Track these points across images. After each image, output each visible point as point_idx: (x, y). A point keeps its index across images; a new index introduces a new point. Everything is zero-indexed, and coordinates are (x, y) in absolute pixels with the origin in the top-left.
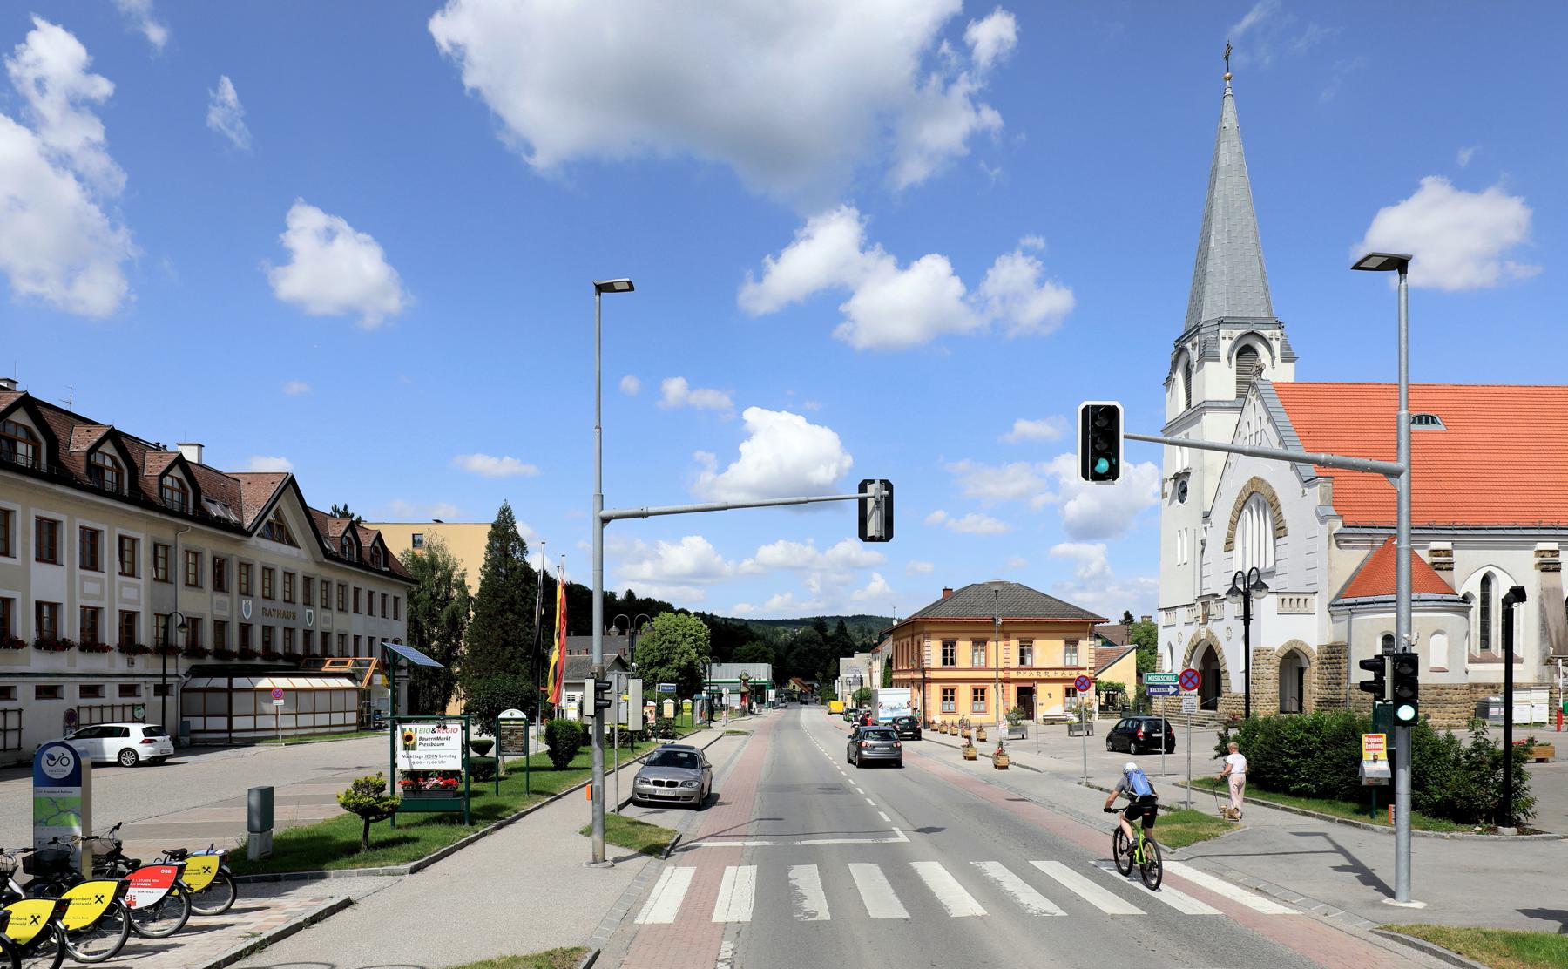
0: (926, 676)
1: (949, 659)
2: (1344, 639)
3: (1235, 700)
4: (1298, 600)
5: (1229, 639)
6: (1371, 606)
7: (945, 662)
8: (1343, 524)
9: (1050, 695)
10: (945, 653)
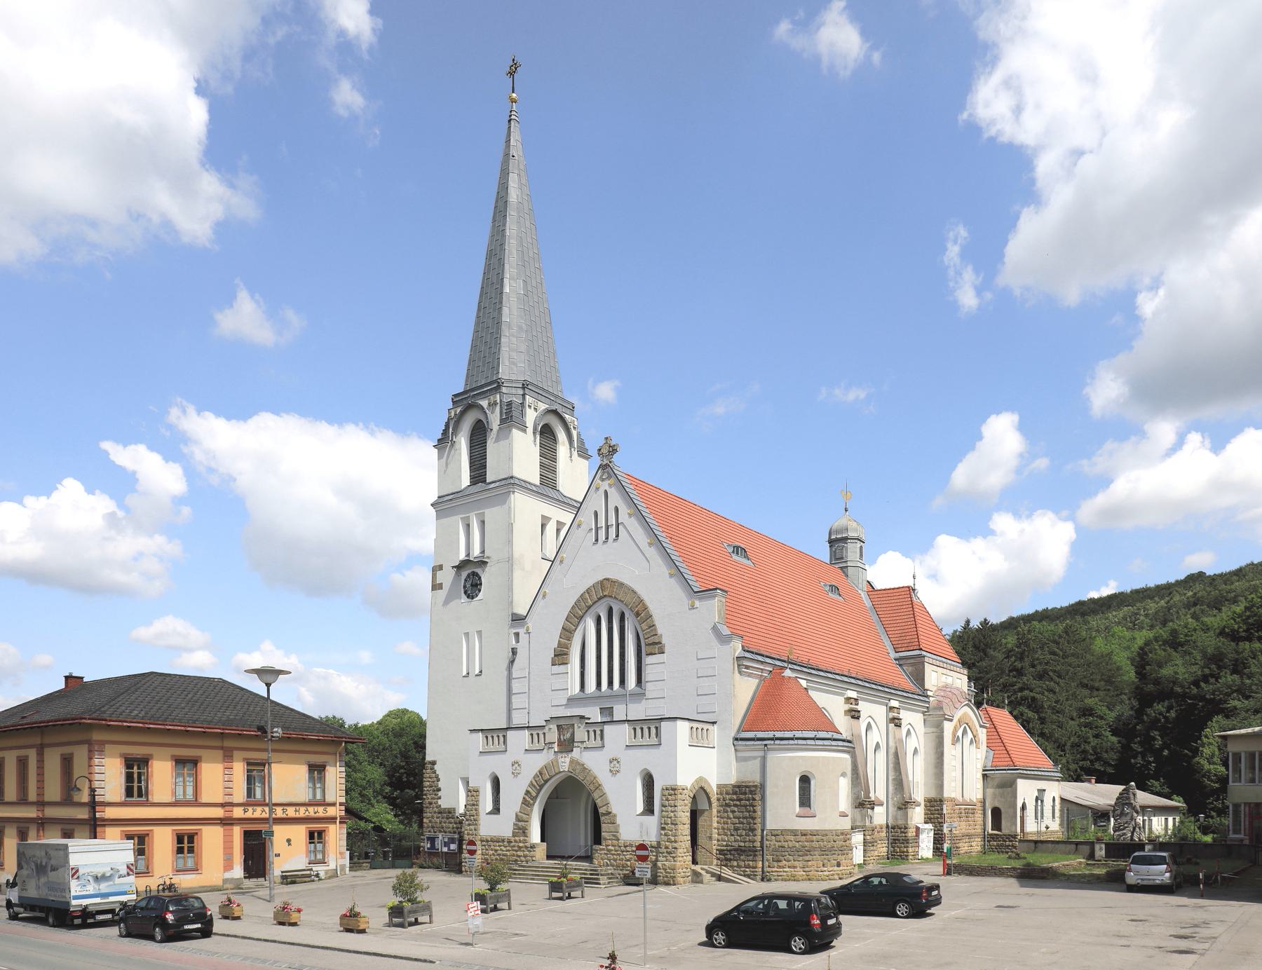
0: (98, 815)
1: (135, 789)
2: (755, 778)
4: (702, 729)
5: (614, 772)
6: (791, 742)
7: (129, 792)
8: (743, 646)
9: (289, 841)
10: (129, 778)
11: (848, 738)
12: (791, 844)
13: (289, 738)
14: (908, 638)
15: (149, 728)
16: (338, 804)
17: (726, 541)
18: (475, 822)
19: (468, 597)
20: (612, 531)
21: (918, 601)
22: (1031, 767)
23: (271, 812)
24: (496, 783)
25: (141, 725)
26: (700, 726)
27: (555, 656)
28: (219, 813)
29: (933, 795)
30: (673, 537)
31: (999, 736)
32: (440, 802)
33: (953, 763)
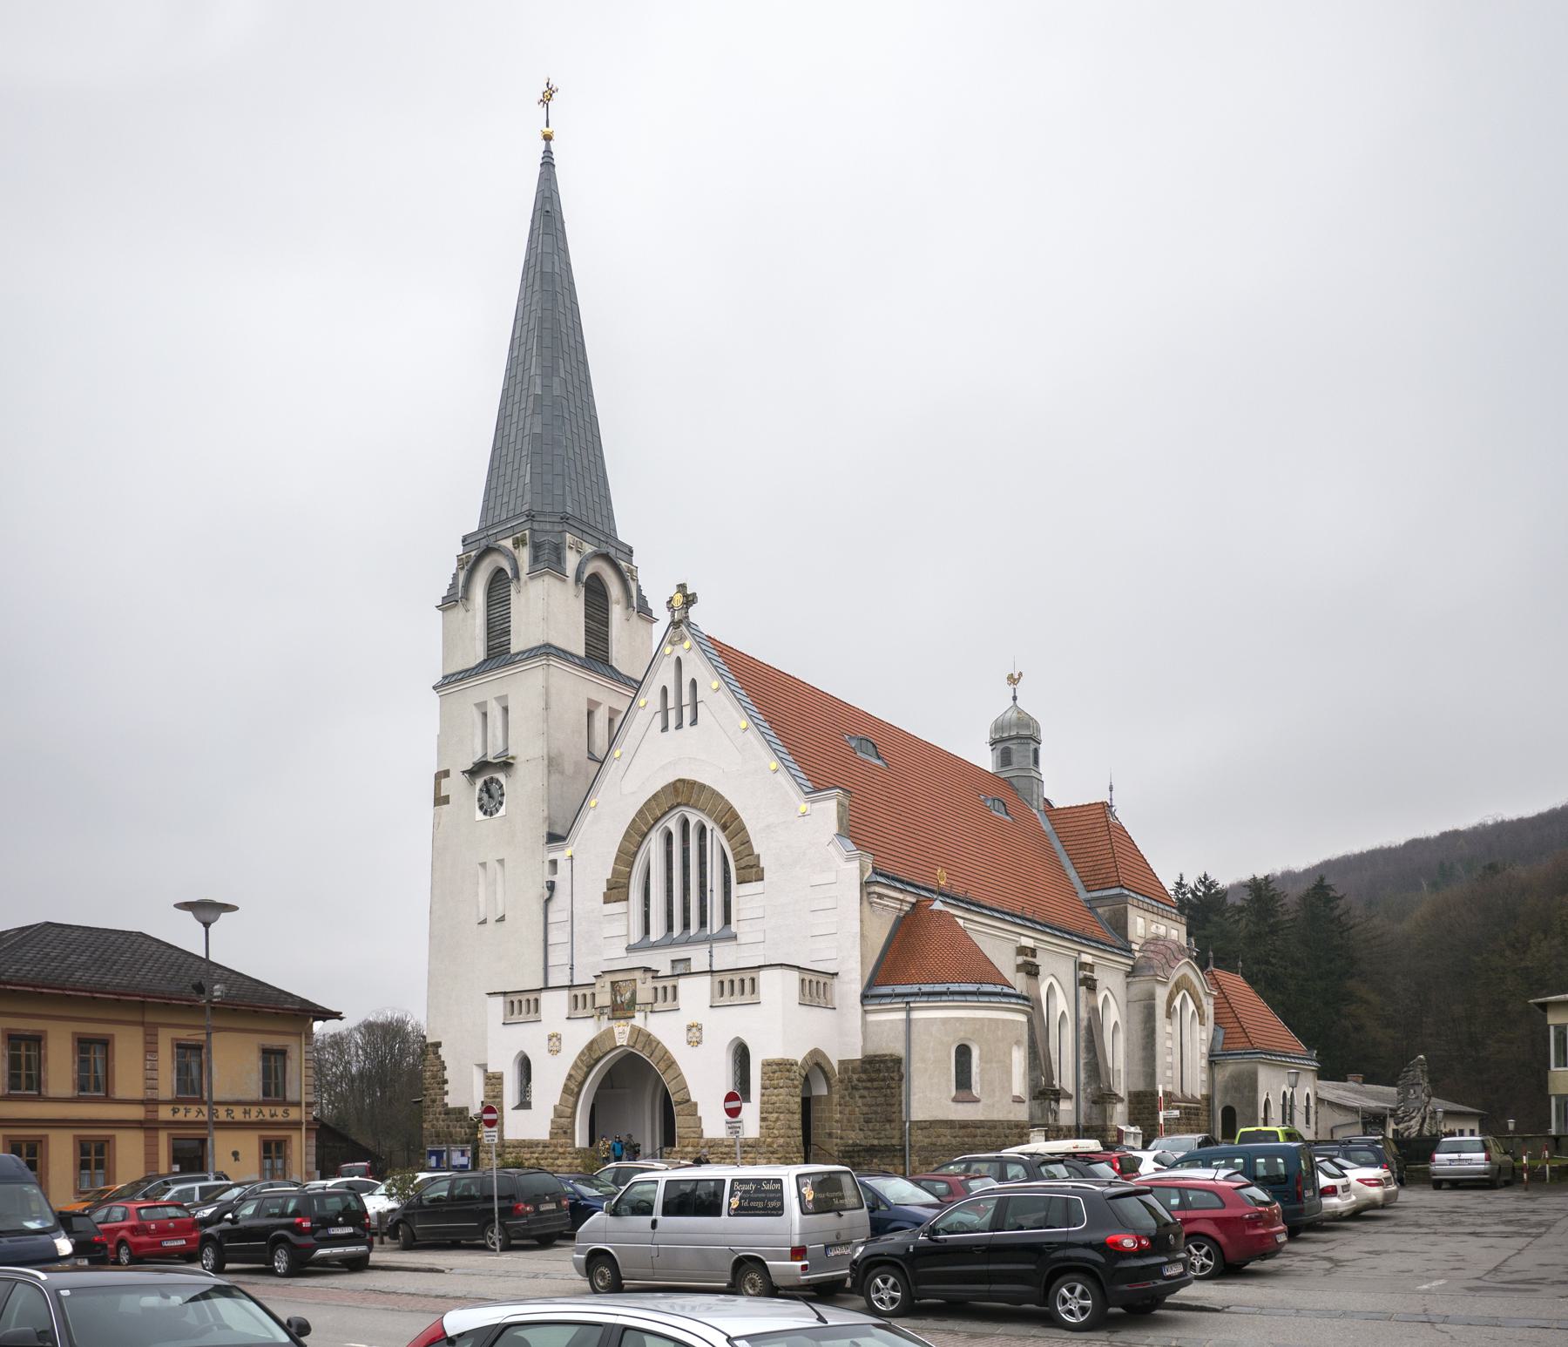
9: (235, 1154)
10: (14, 1063)
11: (1025, 994)
12: (944, 1141)
13: (235, 1010)
14: (1103, 871)
15: (42, 993)
16: (304, 1104)
17: (847, 733)
19: (485, 813)
20: (687, 712)
21: (1117, 822)
22: (1275, 1051)
23: (212, 1113)
24: (525, 1065)
25: (31, 989)
26: (814, 978)
27: (608, 889)
28: (137, 1113)
29: (1140, 1086)
30: (774, 721)
31: (1232, 1008)
32: (447, 1099)
33: (1169, 1044)
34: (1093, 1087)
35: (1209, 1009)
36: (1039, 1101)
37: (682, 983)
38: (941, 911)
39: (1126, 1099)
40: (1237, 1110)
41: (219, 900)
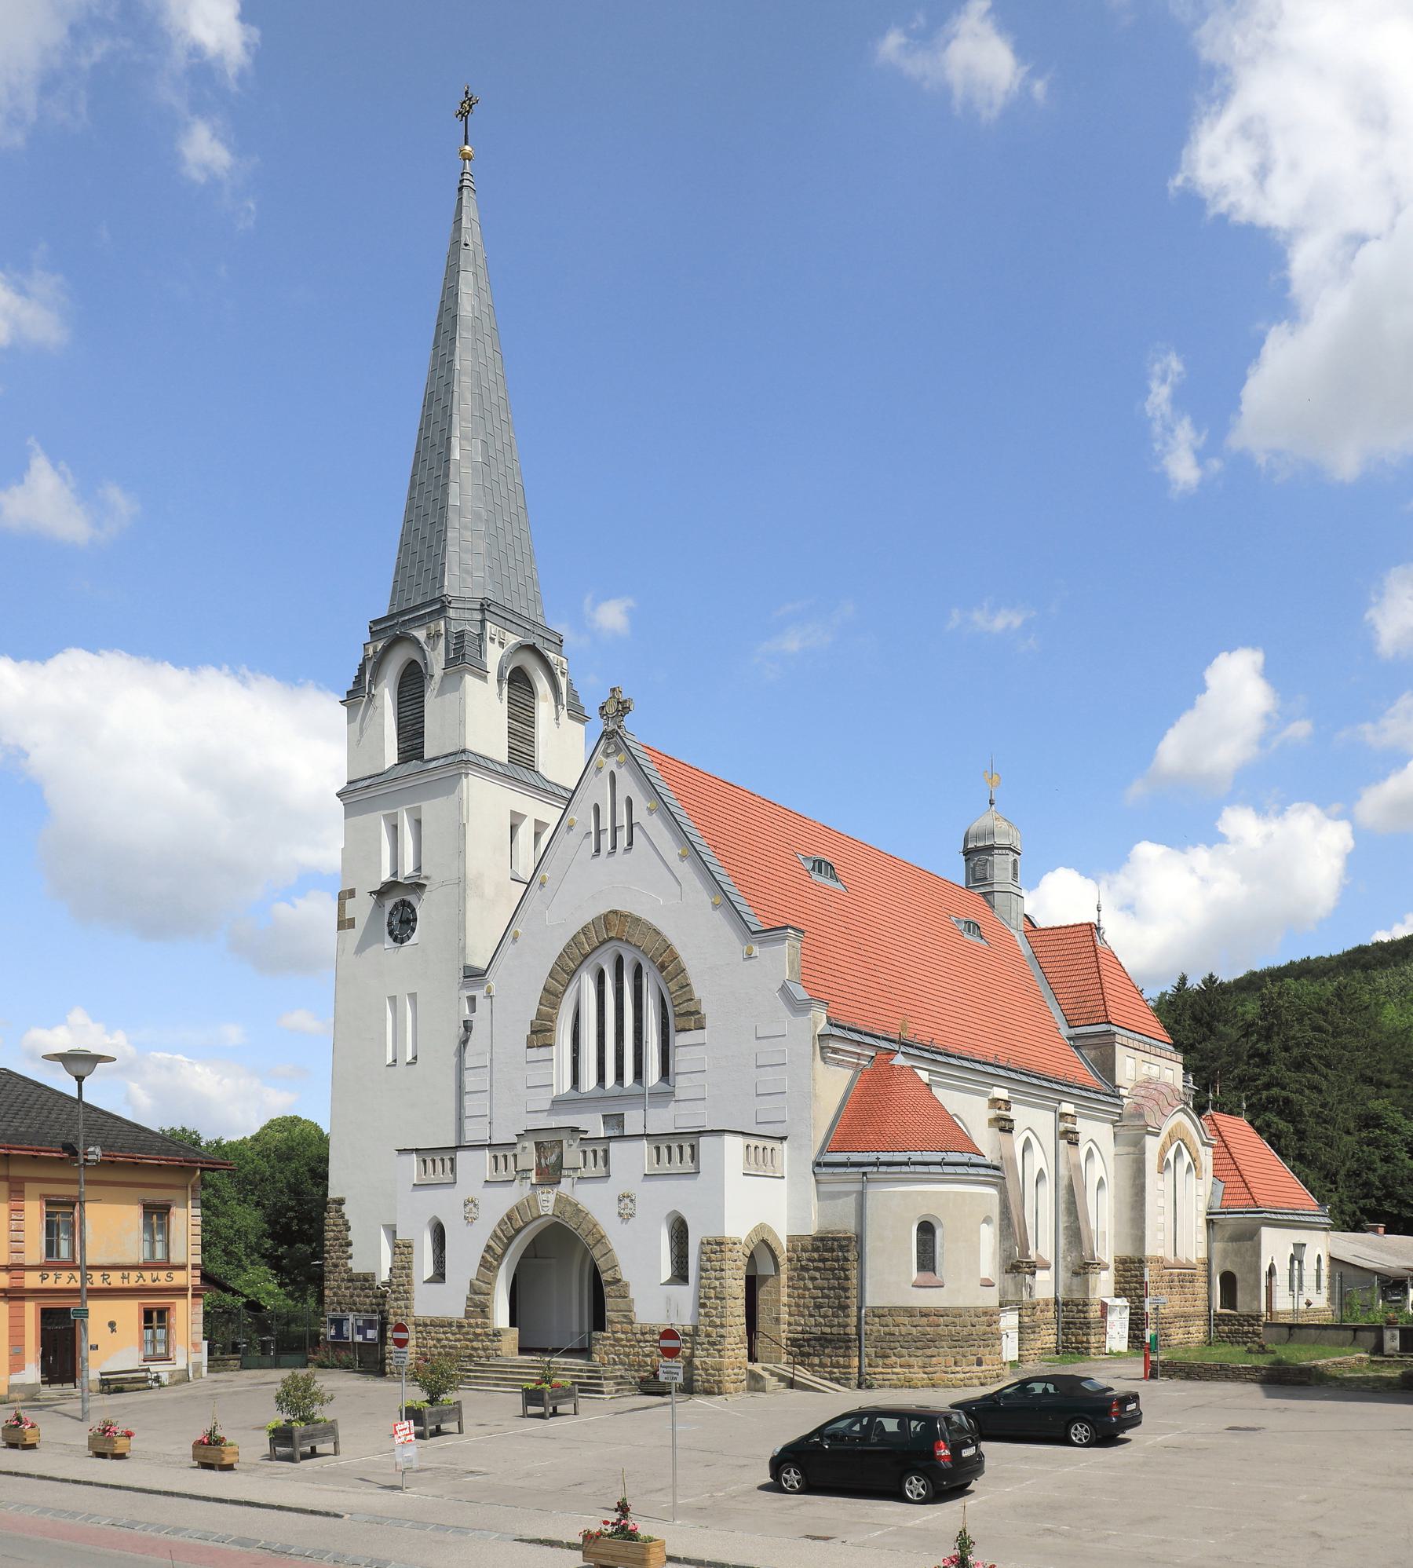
2: (849, 1226)
3: (648, 1337)
5: (625, 1217)
6: (905, 1169)
9: (112, 1325)
11: (995, 1163)
12: (904, 1330)
13: (113, 1162)
14: (1088, 1004)
18: (406, 1296)
19: (395, 940)
22: (1282, 1208)
24: (439, 1234)
26: (761, 1143)
27: (533, 1032)
29: (1127, 1252)
30: (719, 845)
32: (350, 1264)
33: (1161, 1202)
34: (1073, 1255)
35: (1206, 1156)
36: (1011, 1275)
37: (614, 1147)
38: (902, 1067)
39: (1112, 1266)
40: (1238, 1276)
41: (94, 1052)
